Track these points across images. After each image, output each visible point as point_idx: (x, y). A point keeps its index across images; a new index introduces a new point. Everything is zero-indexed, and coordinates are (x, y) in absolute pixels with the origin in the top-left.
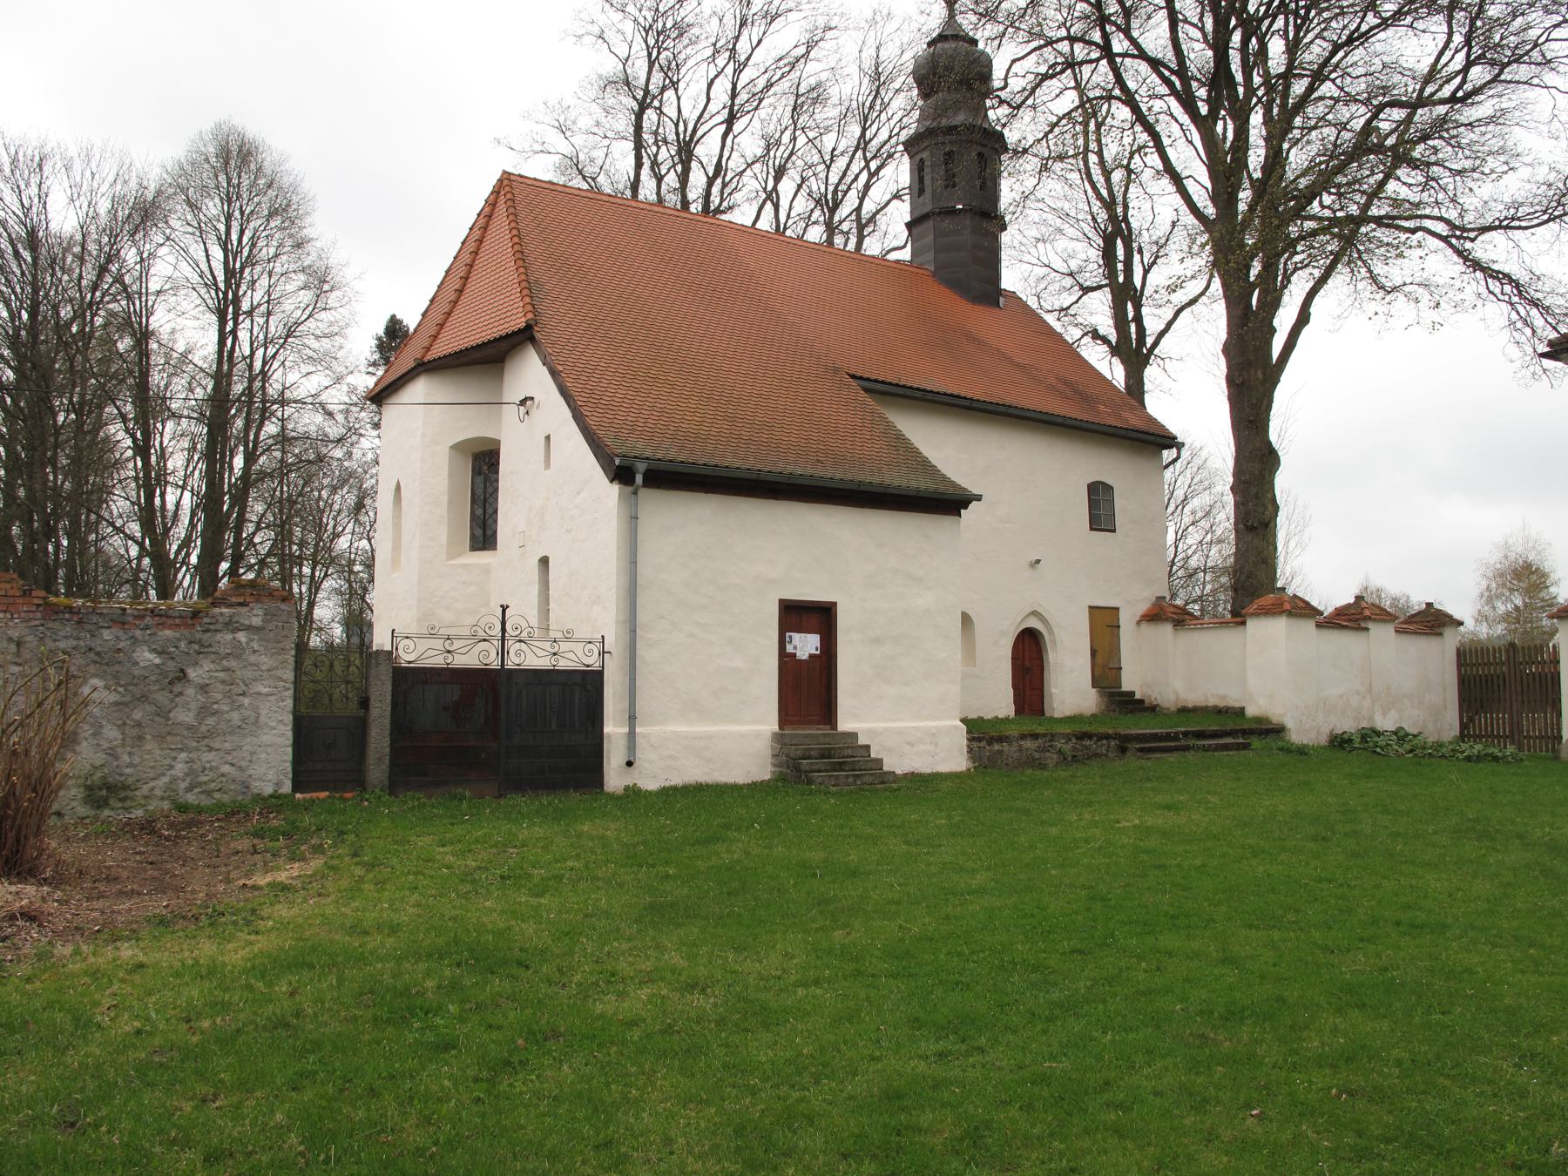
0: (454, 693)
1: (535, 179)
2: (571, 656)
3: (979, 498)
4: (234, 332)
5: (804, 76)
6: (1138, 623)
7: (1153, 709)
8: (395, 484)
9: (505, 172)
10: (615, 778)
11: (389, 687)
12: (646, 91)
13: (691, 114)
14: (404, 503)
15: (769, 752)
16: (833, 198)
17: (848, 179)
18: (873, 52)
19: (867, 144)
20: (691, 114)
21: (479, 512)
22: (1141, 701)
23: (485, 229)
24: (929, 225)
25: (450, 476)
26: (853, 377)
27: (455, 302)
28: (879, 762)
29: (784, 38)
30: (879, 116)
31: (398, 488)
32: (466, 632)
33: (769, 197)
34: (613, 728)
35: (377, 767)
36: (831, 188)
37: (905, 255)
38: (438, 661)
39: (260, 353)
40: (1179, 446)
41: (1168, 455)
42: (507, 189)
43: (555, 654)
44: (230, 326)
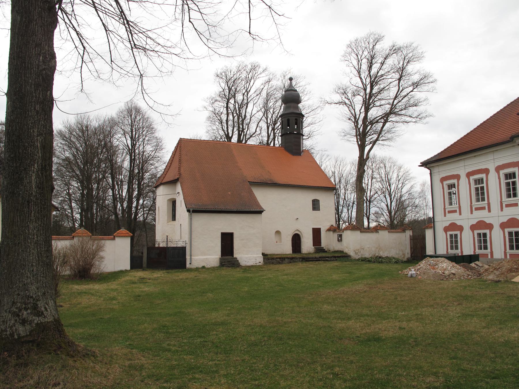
1: (187, 139)
3: (265, 211)
6: (326, 231)
10: (188, 266)
11: (146, 250)
15: (219, 262)
24: (284, 137)
34: (188, 257)
35: (145, 265)
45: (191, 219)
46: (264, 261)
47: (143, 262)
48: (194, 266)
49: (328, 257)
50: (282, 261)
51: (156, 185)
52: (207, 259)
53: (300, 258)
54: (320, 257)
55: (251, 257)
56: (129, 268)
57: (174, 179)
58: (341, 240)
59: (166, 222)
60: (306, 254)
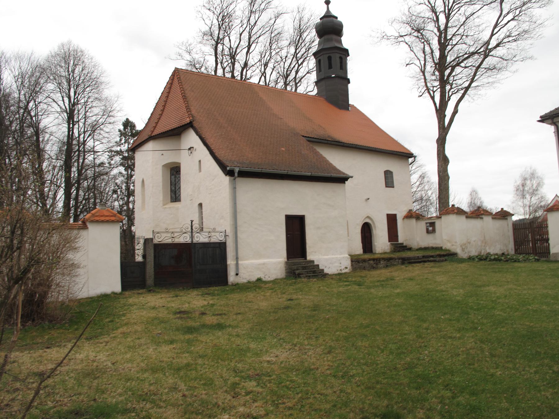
0: (175, 252)
2: (215, 237)
3: (352, 177)
4: (73, 128)
5: (273, 30)
6: (403, 219)
7: (410, 249)
8: (141, 180)
9: (176, 68)
10: (232, 278)
12: (218, 37)
13: (234, 45)
14: (146, 186)
15: (284, 269)
16: (286, 73)
17: (292, 66)
18: (298, 22)
19: (297, 54)
20: (234, 45)
21: (173, 188)
22: (406, 246)
23: (170, 88)
24: (323, 83)
25: (163, 176)
26: (303, 136)
27: (161, 115)
28: (323, 270)
29: (265, 17)
30: (301, 44)
31: (143, 181)
32: (178, 230)
33: (263, 75)
34: (231, 262)
35: (150, 280)
36: (285, 70)
37: (315, 92)
38: (169, 241)
39: (82, 136)
40: (415, 157)
41: (410, 160)
42: (177, 74)
43: (210, 237)
44: (71, 126)
45: (235, 188)
46: (352, 265)
47: (147, 277)
48: (243, 279)
49: (432, 256)
50: (377, 264)
51: (134, 146)
52: (264, 264)
53: (399, 259)
54: (423, 257)
55: (333, 258)
56: (118, 288)
57: (181, 125)
58: (434, 231)
59: (161, 205)
60: (381, 254)
